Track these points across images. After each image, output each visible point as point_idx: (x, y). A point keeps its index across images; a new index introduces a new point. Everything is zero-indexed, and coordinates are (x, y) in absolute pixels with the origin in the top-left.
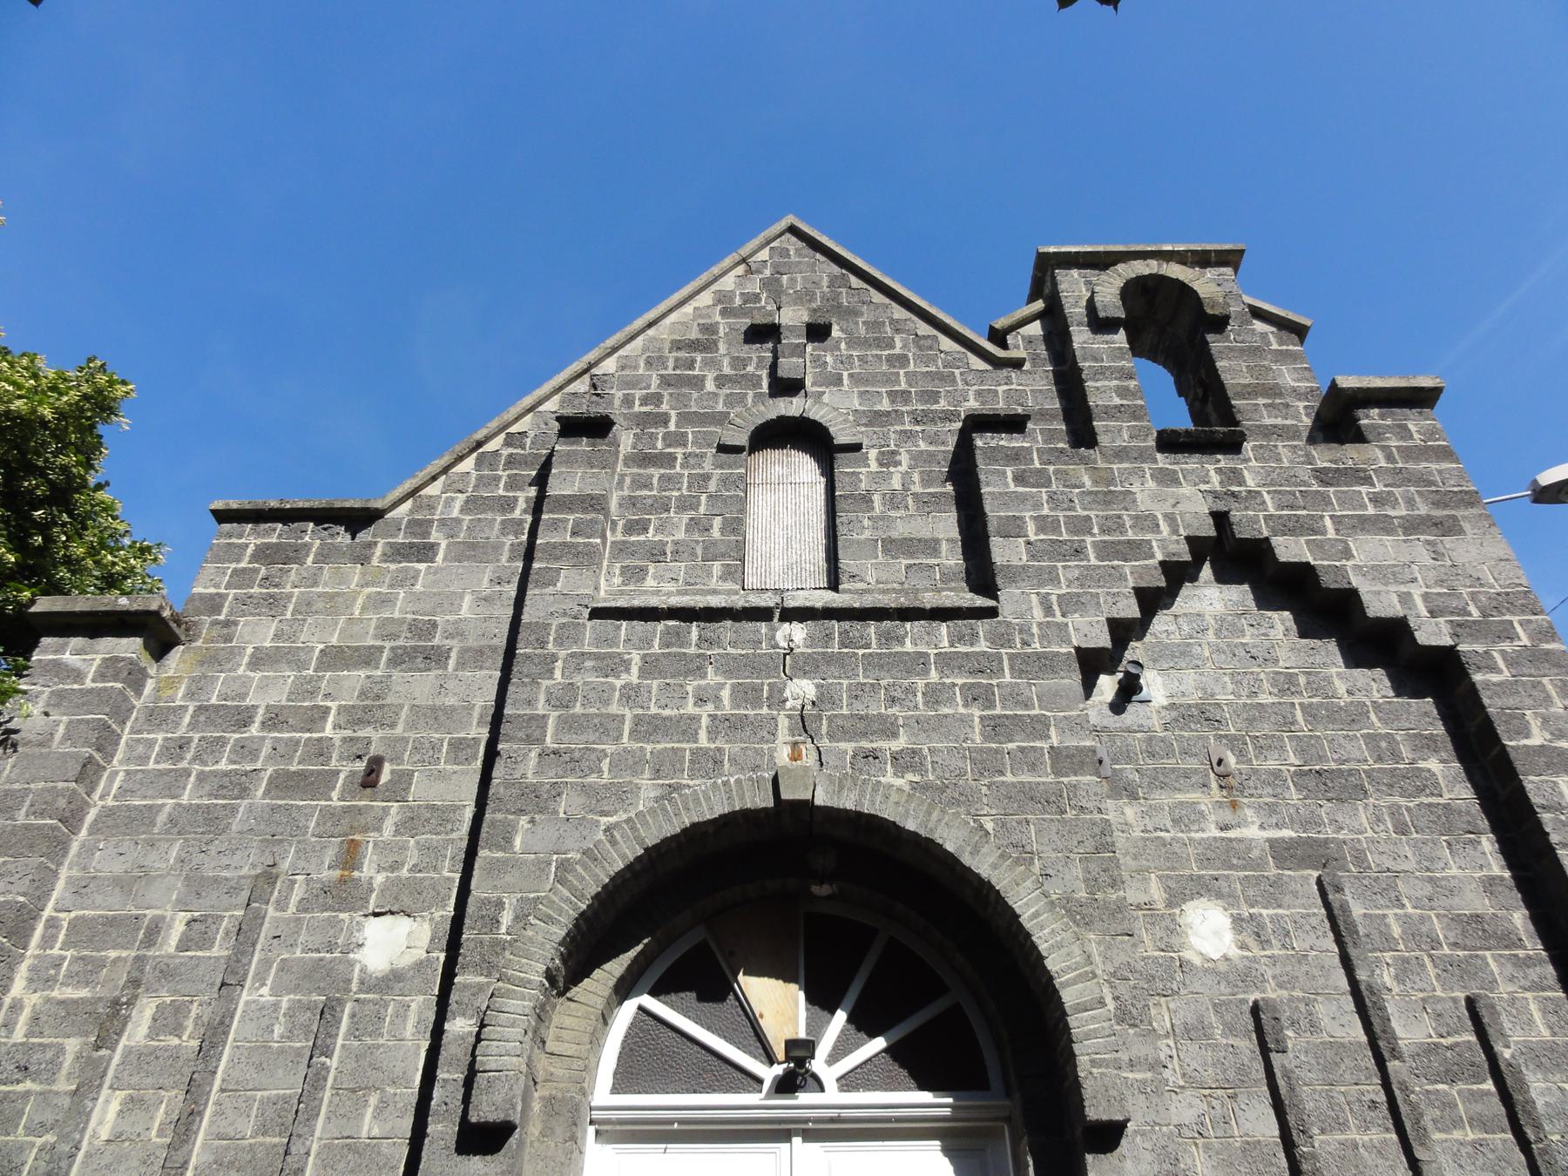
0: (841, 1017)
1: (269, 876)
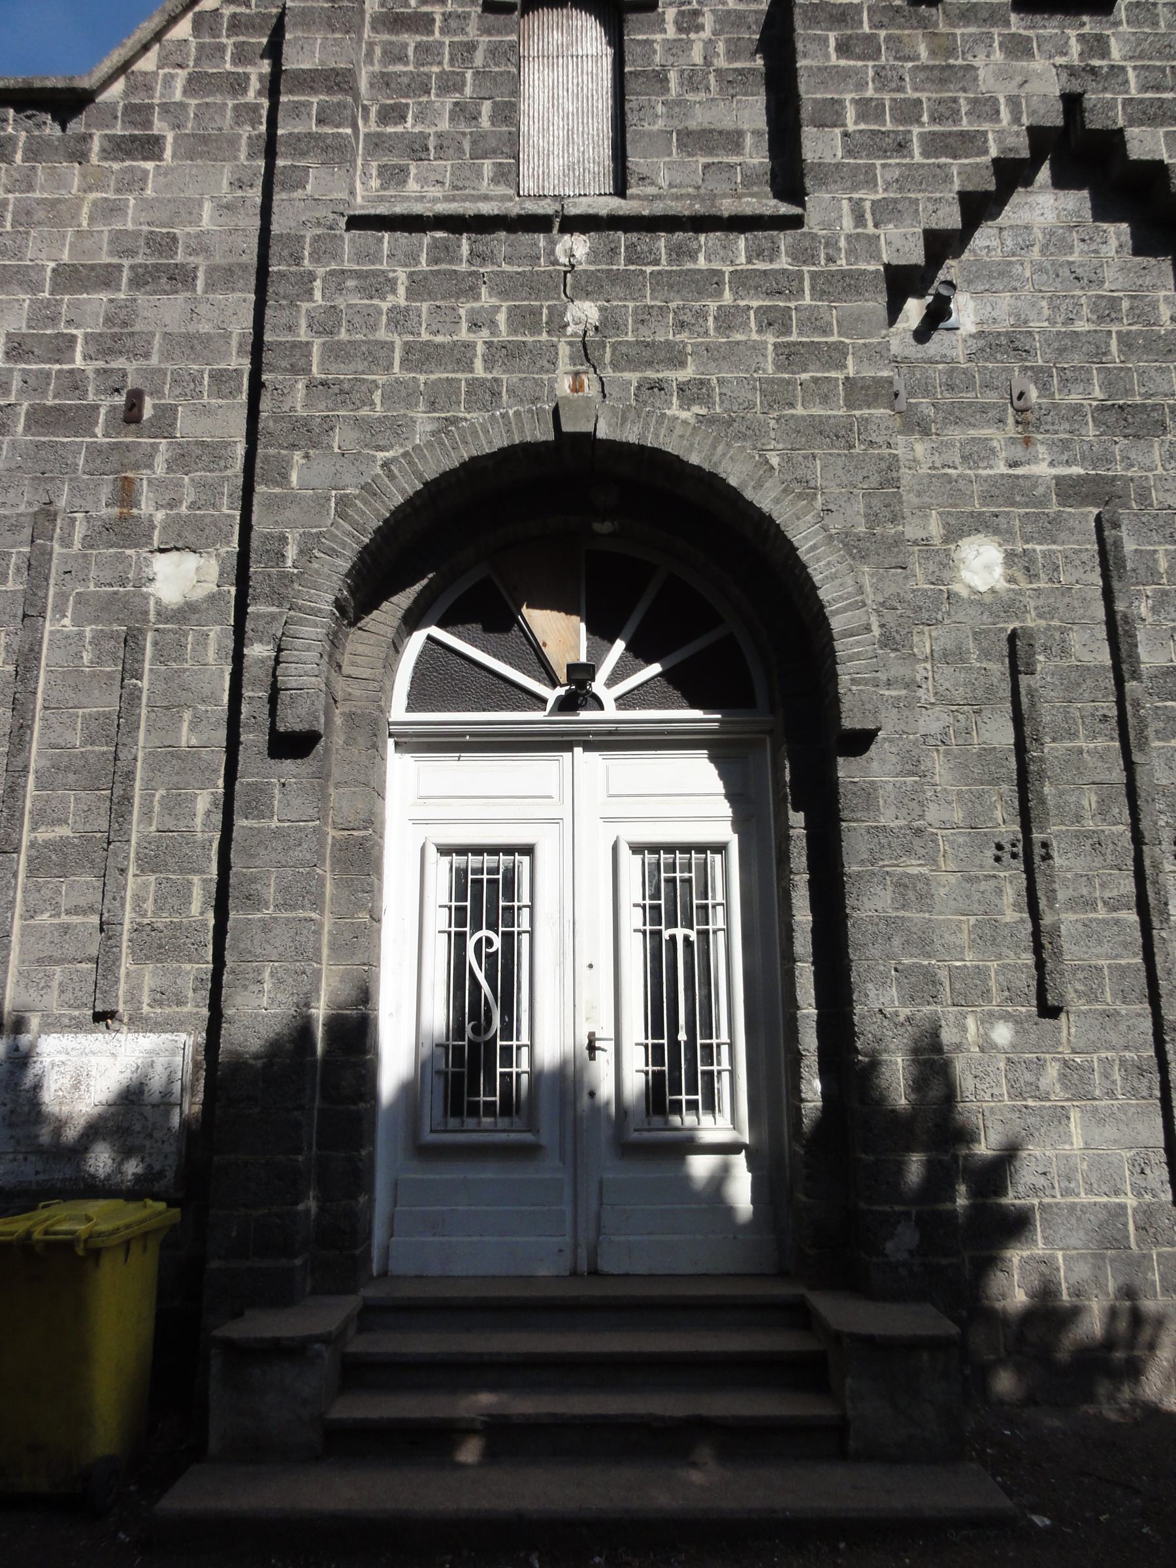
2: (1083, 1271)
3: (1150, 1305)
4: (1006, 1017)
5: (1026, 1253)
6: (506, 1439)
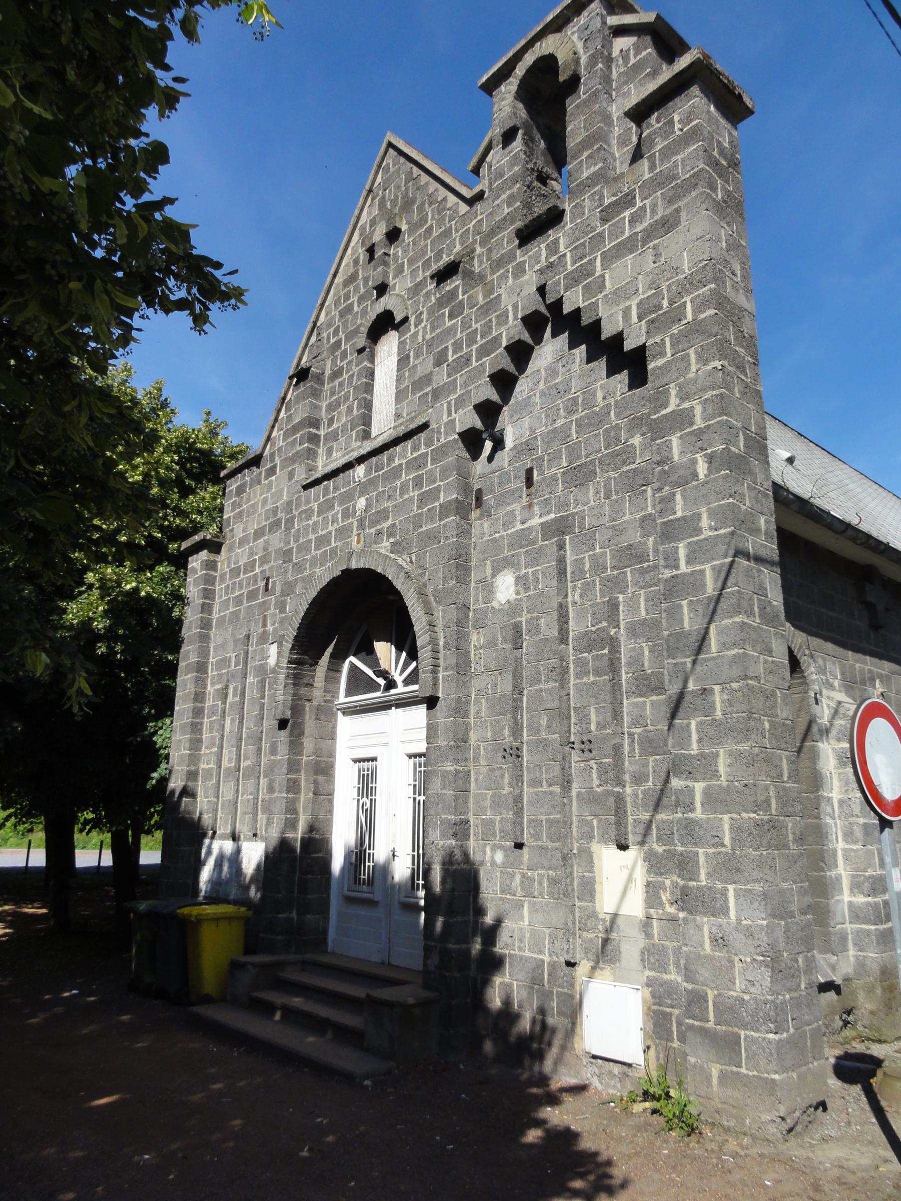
0: (404, 654)
1: (248, 637)
2: (524, 994)
3: (551, 1021)
4: (501, 847)
5: (501, 980)
6: (292, 1016)
